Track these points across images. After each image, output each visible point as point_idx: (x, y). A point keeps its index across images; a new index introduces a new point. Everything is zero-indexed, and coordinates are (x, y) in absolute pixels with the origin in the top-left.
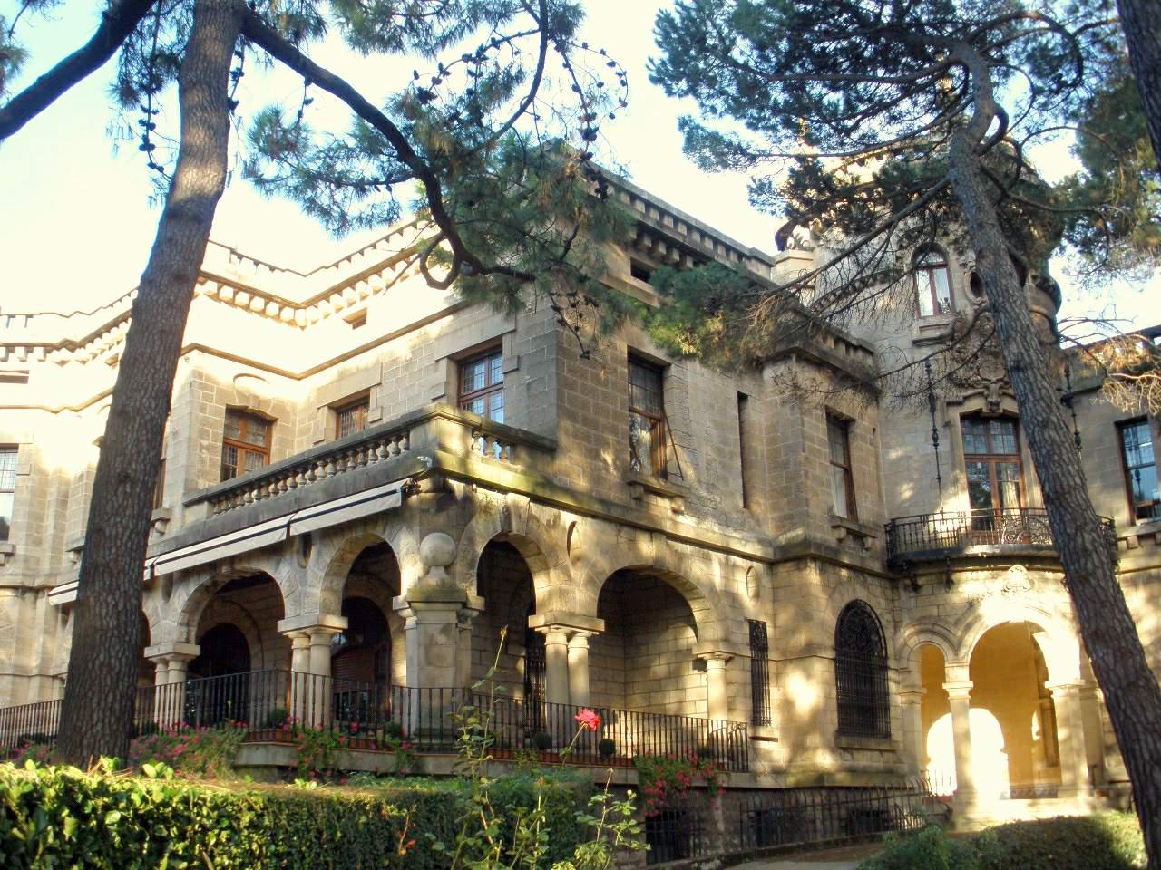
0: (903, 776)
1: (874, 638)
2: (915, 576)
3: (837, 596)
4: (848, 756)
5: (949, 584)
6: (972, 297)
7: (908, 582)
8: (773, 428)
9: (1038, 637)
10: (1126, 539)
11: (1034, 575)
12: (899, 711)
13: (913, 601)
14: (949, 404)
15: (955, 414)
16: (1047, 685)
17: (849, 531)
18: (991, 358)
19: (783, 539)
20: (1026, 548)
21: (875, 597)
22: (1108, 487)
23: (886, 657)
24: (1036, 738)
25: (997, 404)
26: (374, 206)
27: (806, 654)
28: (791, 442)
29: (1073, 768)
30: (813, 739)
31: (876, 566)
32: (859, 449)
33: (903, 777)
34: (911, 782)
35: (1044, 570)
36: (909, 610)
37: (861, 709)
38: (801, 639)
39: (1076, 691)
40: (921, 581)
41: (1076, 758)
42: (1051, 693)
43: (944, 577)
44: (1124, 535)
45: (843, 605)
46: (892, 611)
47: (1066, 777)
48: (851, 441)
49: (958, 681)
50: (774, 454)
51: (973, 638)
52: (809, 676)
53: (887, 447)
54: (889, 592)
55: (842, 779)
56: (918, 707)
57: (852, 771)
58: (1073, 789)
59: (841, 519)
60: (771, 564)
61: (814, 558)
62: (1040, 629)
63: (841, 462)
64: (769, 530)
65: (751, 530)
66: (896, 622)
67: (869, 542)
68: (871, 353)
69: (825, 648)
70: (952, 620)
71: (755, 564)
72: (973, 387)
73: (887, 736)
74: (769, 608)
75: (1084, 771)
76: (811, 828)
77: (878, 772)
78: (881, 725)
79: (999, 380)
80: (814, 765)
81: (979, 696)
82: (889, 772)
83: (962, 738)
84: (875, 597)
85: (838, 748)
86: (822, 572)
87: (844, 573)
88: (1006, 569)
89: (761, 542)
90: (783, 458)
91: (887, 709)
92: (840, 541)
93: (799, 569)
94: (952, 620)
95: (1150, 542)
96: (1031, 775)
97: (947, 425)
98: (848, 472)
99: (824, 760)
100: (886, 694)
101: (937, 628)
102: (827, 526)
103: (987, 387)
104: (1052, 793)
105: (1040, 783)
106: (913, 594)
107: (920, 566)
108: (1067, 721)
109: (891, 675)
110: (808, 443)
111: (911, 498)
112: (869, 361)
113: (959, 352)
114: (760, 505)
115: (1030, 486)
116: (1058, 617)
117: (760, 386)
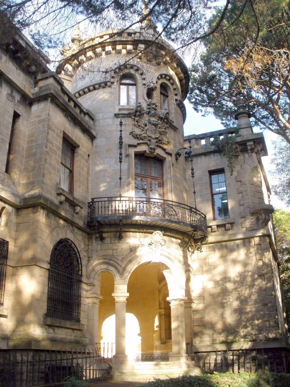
0: (86, 347)
1: (75, 263)
2: (102, 232)
3: (55, 233)
4: (51, 331)
5: (120, 238)
6: (146, 98)
7: (98, 235)
8: (32, 135)
9: (166, 273)
10: (211, 227)
11: (166, 238)
12: (86, 307)
13: (99, 246)
14: (130, 146)
15: (132, 151)
17: (67, 199)
18: (154, 127)
19: (27, 195)
20: (162, 220)
21: (78, 240)
22: (204, 201)
23: (81, 275)
24: (156, 329)
25: (154, 149)
27: (33, 262)
29: (178, 343)
30: (30, 317)
31: (81, 223)
32: (79, 162)
33: (85, 346)
34: (89, 349)
35: (171, 237)
36: (97, 251)
37: (63, 301)
38: (28, 254)
39: (182, 302)
40: (104, 235)
41: (180, 339)
42: (170, 303)
43: (118, 234)
44: (210, 225)
45: (58, 240)
46: (87, 251)
47: (175, 349)
48: (75, 156)
49: (121, 292)
50: (30, 148)
51: (133, 267)
52: (32, 275)
53: (96, 165)
54: (86, 241)
55: (46, 345)
56: (97, 306)
57: (53, 340)
58: (178, 355)
59: (63, 190)
60: (18, 209)
61: (44, 207)
62: (167, 268)
63: (69, 165)
64: (21, 190)
65: (9, 186)
66: (89, 257)
67: (78, 209)
68: (93, 119)
69: (43, 261)
70: (120, 258)
71: (7, 206)
72: (143, 140)
73: (78, 321)
74: (13, 234)
75: (184, 346)
77: (70, 342)
78: (75, 314)
80: (28, 335)
81: (132, 305)
82: (77, 342)
83: (120, 325)
84: (78, 240)
85: (46, 325)
86: (47, 216)
87: (62, 222)
88: (151, 233)
89: (14, 195)
90: (34, 151)
91: (79, 305)
92: (61, 203)
93: (34, 213)
94: (120, 258)
95: (223, 229)
96: (152, 348)
97: (127, 156)
98: (71, 172)
99: (36, 331)
100: (79, 296)
101: (111, 262)
102: (54, 193)
103: (150, 140)
104: (165, 358)
105: (157, 352)
106: (100, 242)
107: (106, 227)
108: (177, 317)
109: (84, 286)
110: (49, 144)
111: (104, 190)
112: (91, 122)
113: (137, 122)
114: (16, 175)
115: (167, 193)
116: (177, 262)
117: (29, 114)
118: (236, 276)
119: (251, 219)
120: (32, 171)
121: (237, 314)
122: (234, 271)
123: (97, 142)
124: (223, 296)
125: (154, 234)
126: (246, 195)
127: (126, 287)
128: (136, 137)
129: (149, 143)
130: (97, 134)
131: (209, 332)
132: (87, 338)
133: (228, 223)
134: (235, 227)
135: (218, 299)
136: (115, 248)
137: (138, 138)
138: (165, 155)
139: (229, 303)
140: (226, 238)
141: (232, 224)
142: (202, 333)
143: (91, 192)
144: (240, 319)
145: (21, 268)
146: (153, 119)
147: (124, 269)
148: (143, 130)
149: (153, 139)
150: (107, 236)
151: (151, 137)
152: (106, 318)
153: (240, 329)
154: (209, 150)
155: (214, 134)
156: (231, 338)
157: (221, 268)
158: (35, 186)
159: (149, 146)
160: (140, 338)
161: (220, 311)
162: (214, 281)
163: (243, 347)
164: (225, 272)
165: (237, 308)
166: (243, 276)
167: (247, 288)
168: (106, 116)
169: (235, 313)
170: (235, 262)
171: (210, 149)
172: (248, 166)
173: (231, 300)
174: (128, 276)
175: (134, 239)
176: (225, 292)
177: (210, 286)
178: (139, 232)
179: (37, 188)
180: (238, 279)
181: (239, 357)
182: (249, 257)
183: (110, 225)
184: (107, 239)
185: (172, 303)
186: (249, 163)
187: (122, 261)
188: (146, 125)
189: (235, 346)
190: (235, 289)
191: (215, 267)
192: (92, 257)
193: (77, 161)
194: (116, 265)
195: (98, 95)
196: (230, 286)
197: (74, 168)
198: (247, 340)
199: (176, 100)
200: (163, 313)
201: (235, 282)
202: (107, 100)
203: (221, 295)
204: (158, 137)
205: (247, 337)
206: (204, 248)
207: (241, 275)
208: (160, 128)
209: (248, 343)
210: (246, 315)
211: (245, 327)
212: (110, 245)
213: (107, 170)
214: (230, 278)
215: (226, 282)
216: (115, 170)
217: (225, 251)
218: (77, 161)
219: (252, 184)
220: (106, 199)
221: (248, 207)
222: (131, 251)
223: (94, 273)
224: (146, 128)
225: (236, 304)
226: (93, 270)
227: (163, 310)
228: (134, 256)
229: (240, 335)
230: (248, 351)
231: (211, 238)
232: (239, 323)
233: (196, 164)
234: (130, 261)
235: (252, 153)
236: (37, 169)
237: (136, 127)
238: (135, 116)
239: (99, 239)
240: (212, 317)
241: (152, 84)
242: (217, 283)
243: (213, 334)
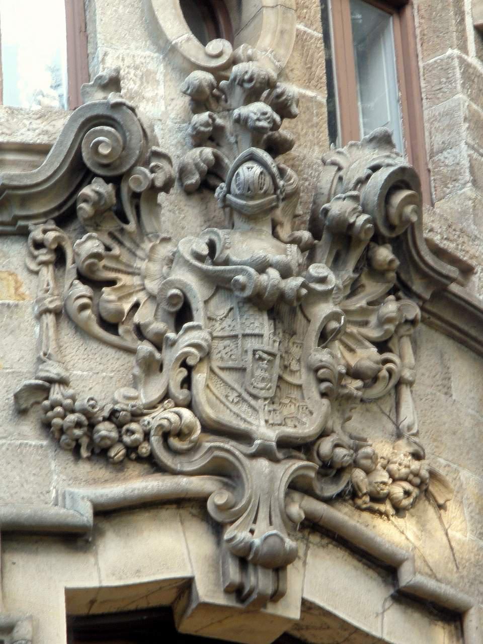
18: (262, 325)
25: (278, 564)
26: (180, 118)
72: (154, 465)
76: (423, 12)
79: (290, 446)
103: (224, 472)
137: (100, 453)
148: (152, 367)
149: (264, 452)
151: (243, 437)
159: (217, 528)
188: (182, 314)
204: (307, 428)
224: (186, 341)
237: (81, 330)
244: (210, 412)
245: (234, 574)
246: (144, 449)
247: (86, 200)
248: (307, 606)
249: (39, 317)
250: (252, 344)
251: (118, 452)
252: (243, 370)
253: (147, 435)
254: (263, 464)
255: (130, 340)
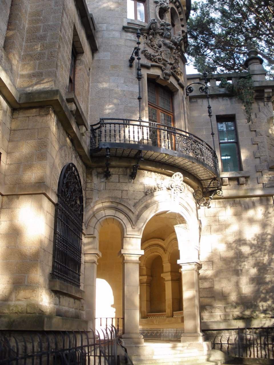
5: (133, 176)
8: (38, 14)
16: (179, 262)
18: (169, 50)
19: (30, 90)
28: (51, 23)
36: (99, 191)
38: (32, 176)
40: (111, 170)
42: (180, 267)
48: (77, 64)
51: (149, 215)
70: (132, 203)
72: (156, 62)
82: (77, 317)
90: (41, 32)
101: (120, 207)
113: (150, 40)
118: (252, 238)
119: (269, 175)
120: (38, 59)
121: (252, 286)
122: (251, 233)
123: (97, 56)
124: (237, 262)
125: (174, 175)
126: (263, 147)
127: (139, 241)
128: (149, 57)
129: (163, 67)
130: (99, 47)
131: (219, 305)
132: (84, 311)
133: (241, 177)
134: (249, 182)
135: (232, 264)
136: (125, 188)
137: (151, 60)
138: (178, 87)
139: (244, 270)
140: (241, 193)
141: (247, 178)
142: (211, 306)
143: (91, 115)
144: (259, 289)
145: (18, 198)
146: (167, 41)
147: (138, 217)
148: (157, 52)
149: (168, 63)
150: (114, 173)
151: (167, 61)
152: (106, 280)
153: (258, 301)
154: (218, 93)
155: (222, 76)
156: (247, 313)
157: (235, 227)
158: (44, 79)
159: (163, 71)
160: (114, 310)
161: (234, 279)
162: (226, 243)
163: (265, 324)
164: (240, 233)
165: (254, 277)
166: (261, 239)
167: (266, 254)
168: (111, 28)
169: (252, 283)
170: (251, 221)
171: (220, 91)
172: (264, 116)
173: (246, 267)
174: (142, 225)
175: (149, 179)
176: (239, 257)
177: (222, 249)
178: (155, 172)
179: (47, 82)
180: (255, 242)
181: (260, 335)
182: (267, 218)
183: (121, 158)
184: (113, 176)
185: (183, 267)
186: (265, 112)
187: (135, 205)
188: (160, 47)
189: (256, 324)
190: (252, 254)
191: (227, 226)
192: (92, 199)
193: (80, 70)
194: (127, 211)
195: (100, 3)
196: (246, 250)
197: (76, 78)
198: (268, 316)
199: (183, 32)
200: (145, 280)
201: (252, 246)
202: (112, 10)
203: (235, 261)
204: (173, 62)
205: (268, 312)
206: (213, 203)
207: (258, 238)
208: (174, 53)
209: (270, 320)
210: (265, 286)
211: (265, 300)
212: (118, 184)
213: (113, 90)
214: (245, 240)
215: (240, 245)
216: (124, 91)
217: (239, 208)
218: (80, 70)
219: (268, 136)
220: (122, 122)
221: (266, 161)
222: (146, 195)
223: (94, 220)
224: (161, 49)
225: (254, 271)
226: (94, 216)
227: (146, 277)
228: (149, 201)
229: (259, 310)
230: (270, 330)
231: (225, 191)
232: (257, 294)
233: (202, 106)
234: (146, 207)
235: (268, 101)
236: (46, 56)
237: (149, 46)
238: (148, 34)
239: (102, 176)
240: (225, 285)
241: (165, 4)
242: (229, 246)
243: (225, 308)
244: (164, 58)
245: (165, 76)
246: (156, 60)
247: (151, 32)
248: (171, 82)
249: (144, 44)
250: (168, 52)
251: (153, 60)
252: (167, 54)
253: (156, 59)
254: (168, 65)
255: (154, 48)
